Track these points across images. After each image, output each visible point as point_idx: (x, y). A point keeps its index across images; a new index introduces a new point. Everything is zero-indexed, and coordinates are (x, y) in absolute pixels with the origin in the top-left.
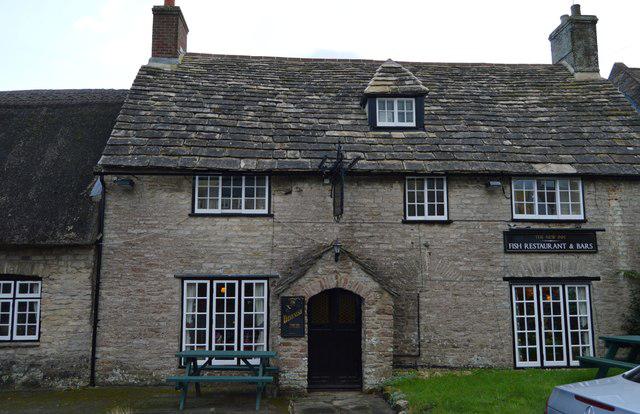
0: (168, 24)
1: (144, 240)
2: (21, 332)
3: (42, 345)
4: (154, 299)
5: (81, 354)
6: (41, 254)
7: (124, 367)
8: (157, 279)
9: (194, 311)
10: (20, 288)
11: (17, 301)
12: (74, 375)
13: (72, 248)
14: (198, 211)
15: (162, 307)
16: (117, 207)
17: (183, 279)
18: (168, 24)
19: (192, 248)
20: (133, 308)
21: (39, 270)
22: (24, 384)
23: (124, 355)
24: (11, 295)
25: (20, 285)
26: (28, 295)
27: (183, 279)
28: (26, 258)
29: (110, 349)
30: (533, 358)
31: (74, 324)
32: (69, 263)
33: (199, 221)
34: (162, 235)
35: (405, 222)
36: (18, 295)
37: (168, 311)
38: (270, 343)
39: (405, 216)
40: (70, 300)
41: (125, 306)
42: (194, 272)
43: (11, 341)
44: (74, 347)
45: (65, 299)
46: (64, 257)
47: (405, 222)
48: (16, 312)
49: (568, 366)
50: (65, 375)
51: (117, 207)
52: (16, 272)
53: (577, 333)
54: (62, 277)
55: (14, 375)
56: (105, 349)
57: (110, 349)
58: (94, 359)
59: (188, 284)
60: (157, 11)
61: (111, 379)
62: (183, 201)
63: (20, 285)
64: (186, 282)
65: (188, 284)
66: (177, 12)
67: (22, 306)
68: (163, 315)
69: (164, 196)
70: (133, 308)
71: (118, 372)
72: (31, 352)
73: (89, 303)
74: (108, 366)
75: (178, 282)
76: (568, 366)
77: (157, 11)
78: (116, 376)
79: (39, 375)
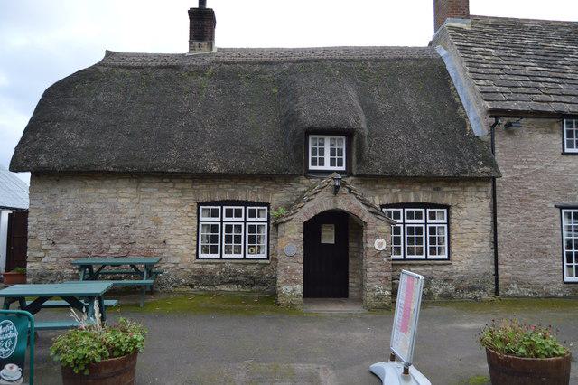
0: (202, 22)
1: (527, 175)
2: (411, 252)
3: (453, 263)
4: (540, 225)
5: (484, 271)
6: (449, 186)
7: (520, 283)
8: (540, 208)
9: (208, 231)
10: (408, 215)
11: (224, 224)
12: (480, 289)
13: (475, 181)
14: (567, 150)
15: (547, 232)
16: (502, 147)
17: (561, 208)
18: (202, 22)
19: (566, 182)
20: (522, 232)
21: (448, 200)
22: (441, 296)
23: (519, 272)
24: (401, 221)
25: (250, 210)
26: (256, 219)
27: (561, 208)
28: (438, 189)
29: (507, 267)
30: (214, 250)
31: (479, 245)
32: (473, 194)
33: (570, 159)
34: (541, 171)
35: (564, 154)
36: (407, 221)
37: (553, 236)
38: (271, 247)
39: (564, 150)
40: (475, 226)
41: (517, 231)
42: (570, 203)
43: (404, 259)
44: (478, 265)
45: (471, 224)
46: (469, 189)
47: (564, 154)
48: (247, 234)
49: (244, 258)
50: (472, 289)
51: (502, 147)
52: (430, 201)
53: (571, 240)
54: (469, 206)
55: (432, 289)
56: (503, 267)
57: (507, 267)
58: (496, 275)
59: (203, 209)
60: (192, 13)
61: (510, 292)
62: (555, 141)
63: (250, 210)
64: (563, 211)
65: (203, 209)
66: (211, 13)
67: (229, 229)
68: (548, 238)
69: (540, 137)
70: (522, 232)
71: (515, 286)
72: (446, 269)
73: (489, 228)
74: (507, 281)
75: (559, 210)
76: (221, 258)
77: (192, 13)
78: (514, 290)
79: (451, 288)
